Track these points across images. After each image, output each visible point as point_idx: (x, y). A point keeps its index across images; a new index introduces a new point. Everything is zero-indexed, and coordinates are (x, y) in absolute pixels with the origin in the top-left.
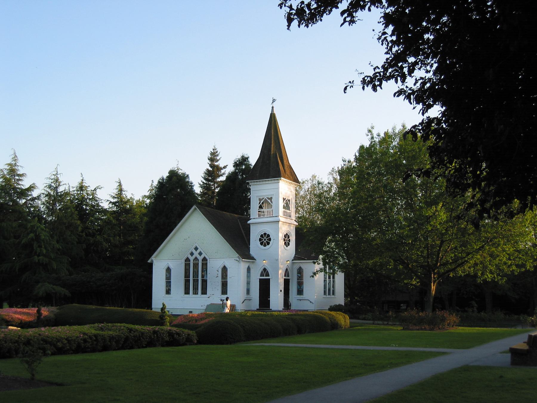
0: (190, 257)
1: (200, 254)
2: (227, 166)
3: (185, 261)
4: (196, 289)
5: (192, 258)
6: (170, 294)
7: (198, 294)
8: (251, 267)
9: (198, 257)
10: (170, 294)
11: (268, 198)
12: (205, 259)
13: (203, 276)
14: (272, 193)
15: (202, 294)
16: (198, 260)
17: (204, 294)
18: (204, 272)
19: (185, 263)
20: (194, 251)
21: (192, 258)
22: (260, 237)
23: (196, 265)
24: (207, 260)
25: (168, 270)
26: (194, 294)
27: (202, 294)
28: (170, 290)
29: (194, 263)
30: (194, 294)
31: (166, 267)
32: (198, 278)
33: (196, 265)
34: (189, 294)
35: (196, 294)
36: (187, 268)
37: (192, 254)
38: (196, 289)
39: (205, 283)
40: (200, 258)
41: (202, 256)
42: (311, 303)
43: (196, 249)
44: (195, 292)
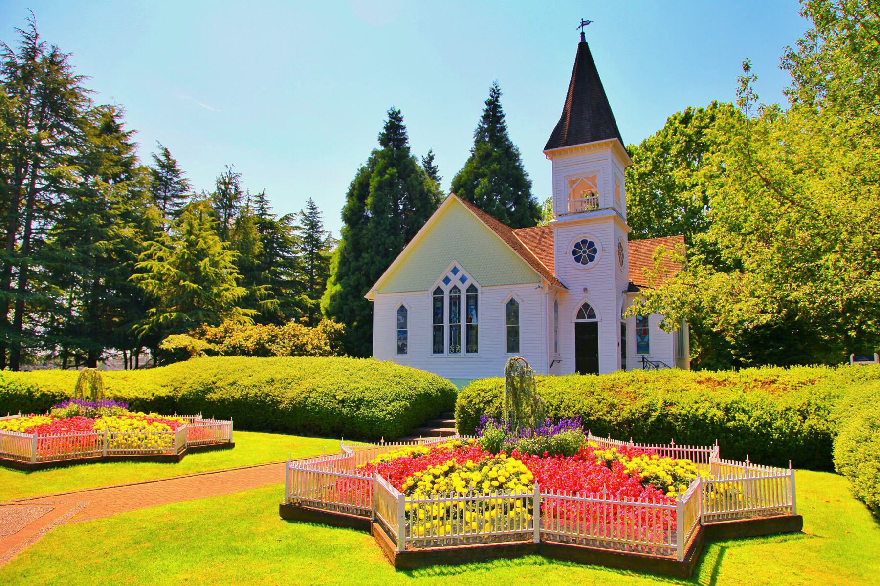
0: (443, 286)
1: (463, 280)
4: (455, 344)
5: (446, 289)
6: (406, 353)
9: (460, 285)
12: (472, 289)
13: (469, 320)
15: (468, 351)
16: (459, 291)
19: (467, 296)
20: (451, 276)
24: (476, 290)
25: (512, 310)
27: (468, 351)
28: (406, 346)
30: (451, 351)
32: (459, 322)
35: (455, 352)
37: (447, 280)
40: (463, 288)
41: (467, 284)
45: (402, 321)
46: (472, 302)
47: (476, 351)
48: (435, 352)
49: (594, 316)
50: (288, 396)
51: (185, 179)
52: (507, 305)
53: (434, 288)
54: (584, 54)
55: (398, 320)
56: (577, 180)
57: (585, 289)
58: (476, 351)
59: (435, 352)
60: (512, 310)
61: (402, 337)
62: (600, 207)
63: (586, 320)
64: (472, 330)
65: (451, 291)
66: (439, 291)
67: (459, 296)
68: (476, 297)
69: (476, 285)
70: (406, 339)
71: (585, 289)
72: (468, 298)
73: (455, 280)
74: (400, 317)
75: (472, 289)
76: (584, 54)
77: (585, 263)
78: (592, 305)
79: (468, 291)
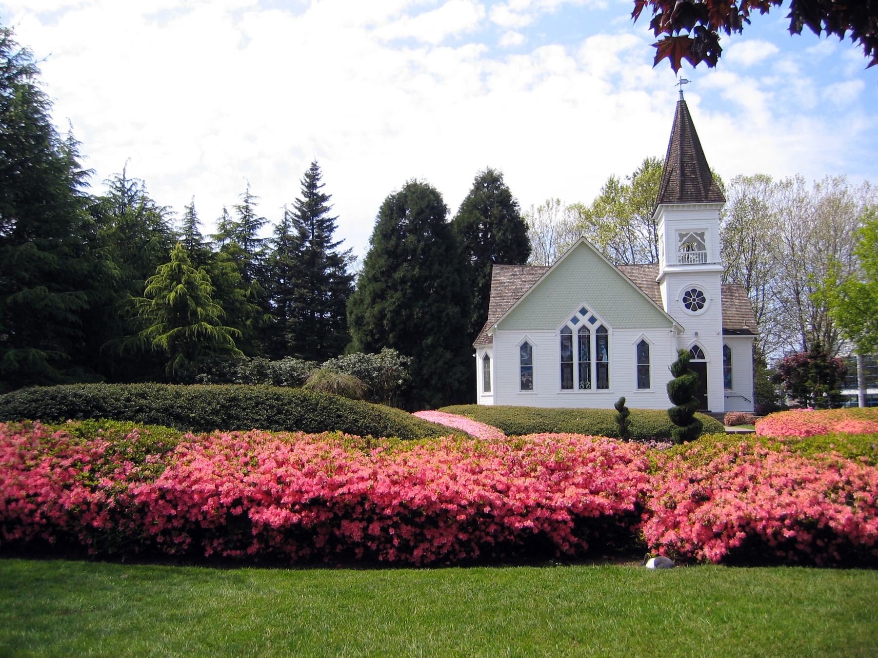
0: (571, 325)
1: (592, 320)
2: (312, 179)
3: (562, 332)
4: (585, 380)
5: (575, 328)
6: (532, 389)
7: (589, 387)
8: (730, 345)
9: (589, 325)
10: (532, 389)
11: (696, 234)
12: (602, 330)
13: (599, 358)
14: (705, 226)
15: (598, 387)
16: (589, 331)
17: (567, 388)
18: (602, 349)
19: (597, 336)
20: (588, 316)
21: (575, 328)
22: (684, 296)
23: (584, 340)
24: (606, 331)
25: (643, 349)
26: (581, 387)
27: (598, 387)
28: (531, 382)
29: (579, 336)
30: (581, 387)
31: (522, 343)
32: (589, 360)
33: (584, 340)
34: (572, 387)
35: (585, 388)
36: (567, 343)
37: (575, 320)
38: (585, 380)
39: (605, 369)
40: (593, 328)
41: (597, 325)
42: (747, 402)
43: (584, 312)
44: (585, 383)
45: (526, 358)
46: (602, 342)
47: (607, 387)
48: (563, 387)
49: (703, 357)
50: (581, 413)
51: (303, 184)
52: (638, 346)
53: (562, 326)
54: (683, 110)
55: (522, 356)
56: (687, 234)
57: (696, 334)
58: (607, 387)
59: (563, 387)
60: (643, 349)
61: (526, 373)
62: (708, 262)
63: (696, 360)
64: (603, 369)
65: (579, 331)
66: (566, 329)
67: (589, 336)
68: (606, 337)
69: (606, 325)
70: (531, 375)
71: (696, 334)
72: (598, 338)
73: (584, 320)
74: (524, 354)
75: (602, 330)
76: (683, 110)
77: (694, 310)
78: (701, 347)
79: (597, 331)
